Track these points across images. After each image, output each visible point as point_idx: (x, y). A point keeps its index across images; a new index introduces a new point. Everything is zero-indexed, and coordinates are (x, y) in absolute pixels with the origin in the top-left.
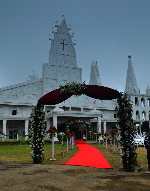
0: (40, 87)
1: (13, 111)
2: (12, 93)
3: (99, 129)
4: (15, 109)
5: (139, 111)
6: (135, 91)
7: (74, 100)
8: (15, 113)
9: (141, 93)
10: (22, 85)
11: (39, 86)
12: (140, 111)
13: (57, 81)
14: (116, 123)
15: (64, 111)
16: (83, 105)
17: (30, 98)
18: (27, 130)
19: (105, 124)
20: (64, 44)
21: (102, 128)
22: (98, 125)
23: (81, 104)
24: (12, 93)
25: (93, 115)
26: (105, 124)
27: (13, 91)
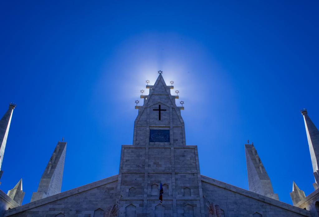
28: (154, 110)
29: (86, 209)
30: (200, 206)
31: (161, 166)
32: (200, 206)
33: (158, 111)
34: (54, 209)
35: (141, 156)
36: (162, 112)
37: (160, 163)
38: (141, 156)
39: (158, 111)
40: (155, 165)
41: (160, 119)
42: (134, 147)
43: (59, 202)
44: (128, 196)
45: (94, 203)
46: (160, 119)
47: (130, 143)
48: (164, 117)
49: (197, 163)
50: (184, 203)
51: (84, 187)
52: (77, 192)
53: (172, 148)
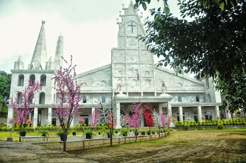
20: (132, 26)
24: (81, 81)
28: (129, 26)
29: (97, 81)
30: (126, 82)
31: (134, 60)
32: (126, 82)
33: (133, 25)
34: (81, 81)
35: (123, 54)
36: (133, 27)
37: (133, 58)
38: (123, 54)
39: (133, 25)
40: (131, 60)
41: (132, 32)
42: (119, 49)
43: (82, 77)
44: (51, 63)
45: (100, 78)
46: (132, 32)
47: (116, 46)
48: (134, 30)
49: (153, 59)
50: (202, 141)
51: (94, 70)
52: (90, 73)
53: (140, 50)
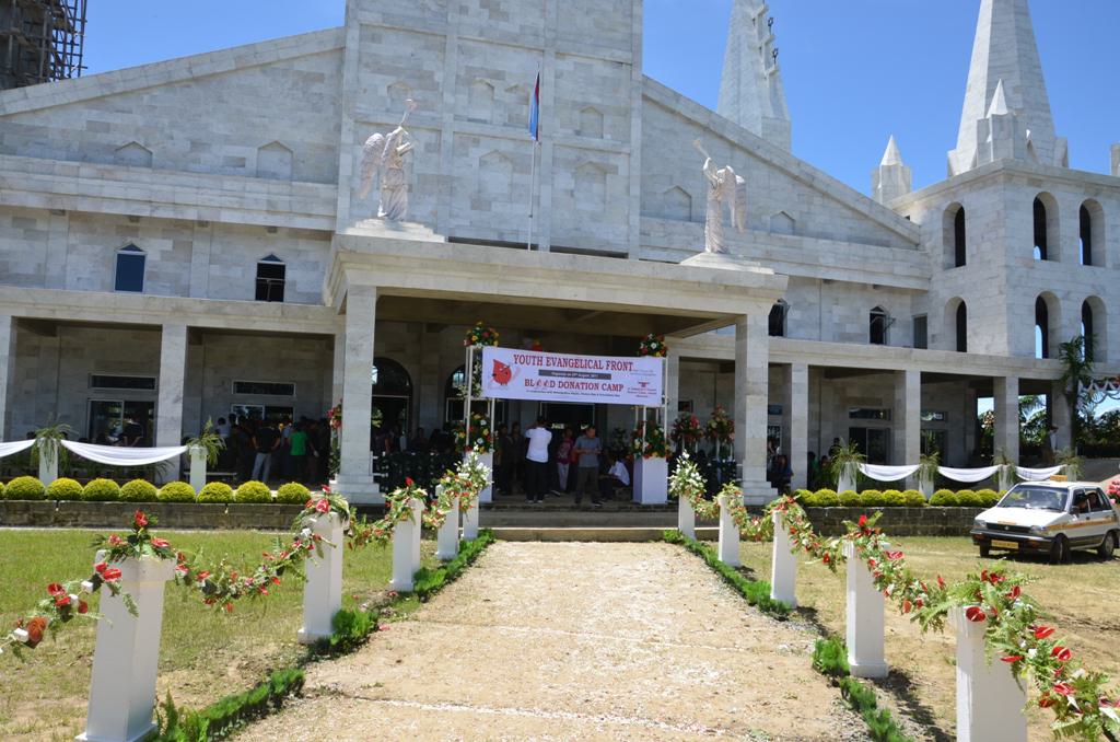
0: (321, 96)
1: (265, 299)
2: (107, 128)
3: (749, 414)
4: (132, 247)
5: (1059, 295)
6: (820, 328)
7: (572, 193)
8: (130, 273)
9: (1075, 164)
10: (190, 70)
11: (316, 88)
12: (1067, 296)
13: (443, 50)
14: (399, 450)
15: (437, 245)
16: (643, 233)
17: (241, 169)
18: (173, 397)
19: (800, 379)
21: (778, 409)
22: (745, 380)
23: (624, 228)
25: (698, 286)
26: (800, 379)
27: (115, 119)
